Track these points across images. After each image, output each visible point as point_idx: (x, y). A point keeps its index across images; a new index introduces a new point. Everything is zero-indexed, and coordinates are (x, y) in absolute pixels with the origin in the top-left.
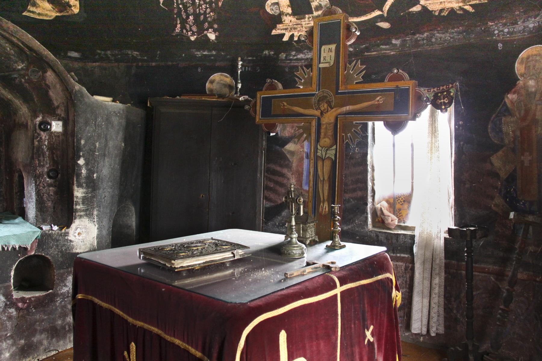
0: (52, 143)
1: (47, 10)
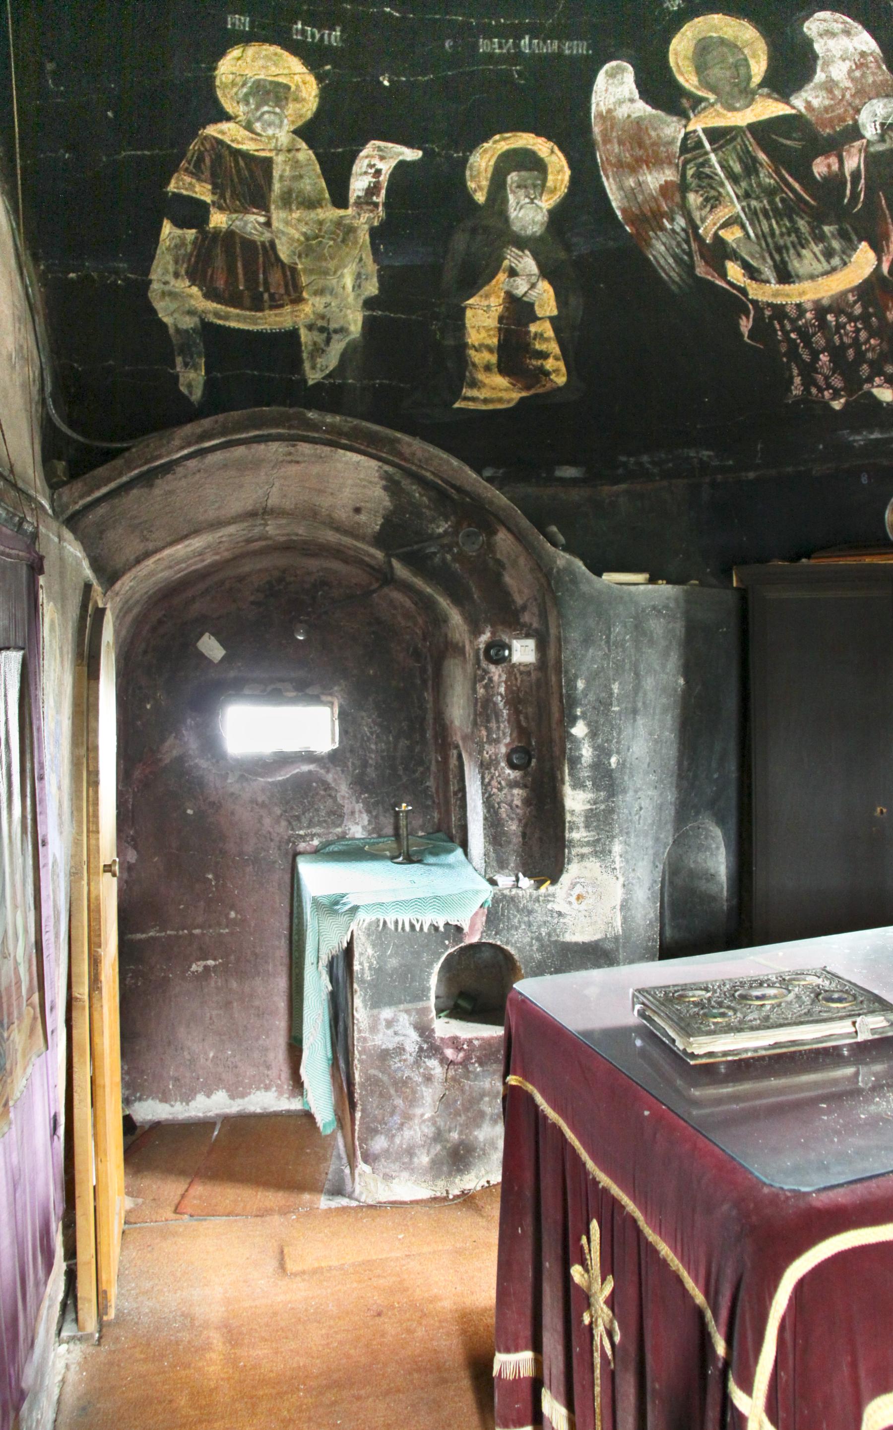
0: (514, 688)
1: (501, 390)
